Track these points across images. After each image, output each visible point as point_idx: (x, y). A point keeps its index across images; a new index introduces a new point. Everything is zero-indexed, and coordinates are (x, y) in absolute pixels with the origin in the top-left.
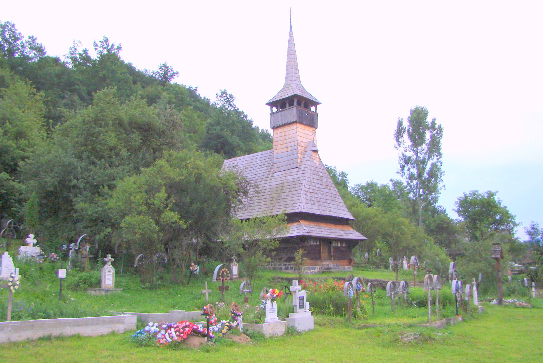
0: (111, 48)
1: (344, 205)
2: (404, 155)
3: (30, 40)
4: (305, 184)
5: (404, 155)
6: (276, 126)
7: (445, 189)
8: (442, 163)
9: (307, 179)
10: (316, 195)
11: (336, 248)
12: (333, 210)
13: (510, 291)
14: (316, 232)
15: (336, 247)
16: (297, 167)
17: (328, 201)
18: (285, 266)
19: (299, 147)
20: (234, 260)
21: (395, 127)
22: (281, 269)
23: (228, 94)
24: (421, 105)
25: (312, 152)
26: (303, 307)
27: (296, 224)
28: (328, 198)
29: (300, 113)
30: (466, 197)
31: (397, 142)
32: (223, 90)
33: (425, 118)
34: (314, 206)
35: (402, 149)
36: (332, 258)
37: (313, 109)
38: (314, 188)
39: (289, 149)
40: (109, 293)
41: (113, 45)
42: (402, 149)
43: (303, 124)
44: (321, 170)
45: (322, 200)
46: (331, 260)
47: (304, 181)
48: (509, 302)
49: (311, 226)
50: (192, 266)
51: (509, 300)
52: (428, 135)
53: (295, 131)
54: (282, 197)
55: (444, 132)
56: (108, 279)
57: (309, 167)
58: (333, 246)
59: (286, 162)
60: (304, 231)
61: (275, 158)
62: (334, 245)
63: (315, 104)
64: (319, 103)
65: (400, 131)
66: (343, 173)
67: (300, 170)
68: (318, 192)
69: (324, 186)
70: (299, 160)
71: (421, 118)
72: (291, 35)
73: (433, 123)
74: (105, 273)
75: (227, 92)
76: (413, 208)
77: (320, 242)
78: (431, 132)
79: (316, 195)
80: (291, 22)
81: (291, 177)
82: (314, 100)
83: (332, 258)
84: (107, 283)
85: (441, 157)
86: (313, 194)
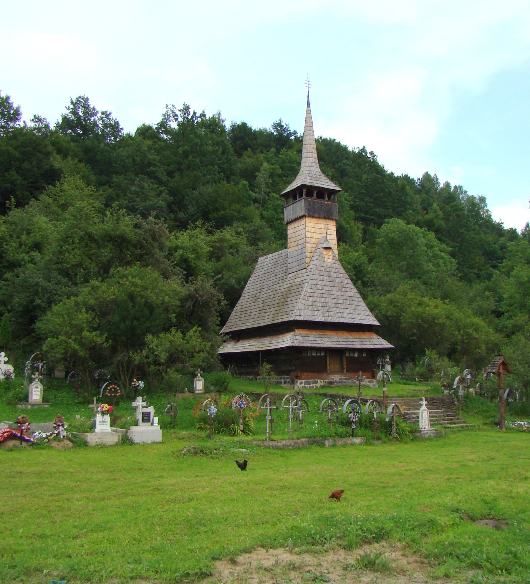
0: (192, 117)
3: (104, 116)
4: (307, 288)
9: (311, 282)
14: (314, 342)
17: (340, 306)
19: (307, 245)
20: (199, 374)
23: (368, 152)
25: (323, 250)
27: (292, 333)
29: (310, 205)
32: (361, 148)
34: (316, 313)
36: (345, 371)
38: (320, 291)
40: (36, 407)
41: (195, 113)
43: (316, 218)
44: (334, 270)
45: (330, 305)
46: (343, 372)
50: (134, 382)
53: (303, 227)
56: (35, 394)
60: (295, 341)
61: (289, 257)
62: (347, 355)
68: (326, 296)
69: (337, 289)
70: (308, 260)
72: (309, 112)
74: (32, 389)
75: (366, 149)
77: (326, 354)
80: (308, 97)
84: (34, 398)
86: (318, 299)
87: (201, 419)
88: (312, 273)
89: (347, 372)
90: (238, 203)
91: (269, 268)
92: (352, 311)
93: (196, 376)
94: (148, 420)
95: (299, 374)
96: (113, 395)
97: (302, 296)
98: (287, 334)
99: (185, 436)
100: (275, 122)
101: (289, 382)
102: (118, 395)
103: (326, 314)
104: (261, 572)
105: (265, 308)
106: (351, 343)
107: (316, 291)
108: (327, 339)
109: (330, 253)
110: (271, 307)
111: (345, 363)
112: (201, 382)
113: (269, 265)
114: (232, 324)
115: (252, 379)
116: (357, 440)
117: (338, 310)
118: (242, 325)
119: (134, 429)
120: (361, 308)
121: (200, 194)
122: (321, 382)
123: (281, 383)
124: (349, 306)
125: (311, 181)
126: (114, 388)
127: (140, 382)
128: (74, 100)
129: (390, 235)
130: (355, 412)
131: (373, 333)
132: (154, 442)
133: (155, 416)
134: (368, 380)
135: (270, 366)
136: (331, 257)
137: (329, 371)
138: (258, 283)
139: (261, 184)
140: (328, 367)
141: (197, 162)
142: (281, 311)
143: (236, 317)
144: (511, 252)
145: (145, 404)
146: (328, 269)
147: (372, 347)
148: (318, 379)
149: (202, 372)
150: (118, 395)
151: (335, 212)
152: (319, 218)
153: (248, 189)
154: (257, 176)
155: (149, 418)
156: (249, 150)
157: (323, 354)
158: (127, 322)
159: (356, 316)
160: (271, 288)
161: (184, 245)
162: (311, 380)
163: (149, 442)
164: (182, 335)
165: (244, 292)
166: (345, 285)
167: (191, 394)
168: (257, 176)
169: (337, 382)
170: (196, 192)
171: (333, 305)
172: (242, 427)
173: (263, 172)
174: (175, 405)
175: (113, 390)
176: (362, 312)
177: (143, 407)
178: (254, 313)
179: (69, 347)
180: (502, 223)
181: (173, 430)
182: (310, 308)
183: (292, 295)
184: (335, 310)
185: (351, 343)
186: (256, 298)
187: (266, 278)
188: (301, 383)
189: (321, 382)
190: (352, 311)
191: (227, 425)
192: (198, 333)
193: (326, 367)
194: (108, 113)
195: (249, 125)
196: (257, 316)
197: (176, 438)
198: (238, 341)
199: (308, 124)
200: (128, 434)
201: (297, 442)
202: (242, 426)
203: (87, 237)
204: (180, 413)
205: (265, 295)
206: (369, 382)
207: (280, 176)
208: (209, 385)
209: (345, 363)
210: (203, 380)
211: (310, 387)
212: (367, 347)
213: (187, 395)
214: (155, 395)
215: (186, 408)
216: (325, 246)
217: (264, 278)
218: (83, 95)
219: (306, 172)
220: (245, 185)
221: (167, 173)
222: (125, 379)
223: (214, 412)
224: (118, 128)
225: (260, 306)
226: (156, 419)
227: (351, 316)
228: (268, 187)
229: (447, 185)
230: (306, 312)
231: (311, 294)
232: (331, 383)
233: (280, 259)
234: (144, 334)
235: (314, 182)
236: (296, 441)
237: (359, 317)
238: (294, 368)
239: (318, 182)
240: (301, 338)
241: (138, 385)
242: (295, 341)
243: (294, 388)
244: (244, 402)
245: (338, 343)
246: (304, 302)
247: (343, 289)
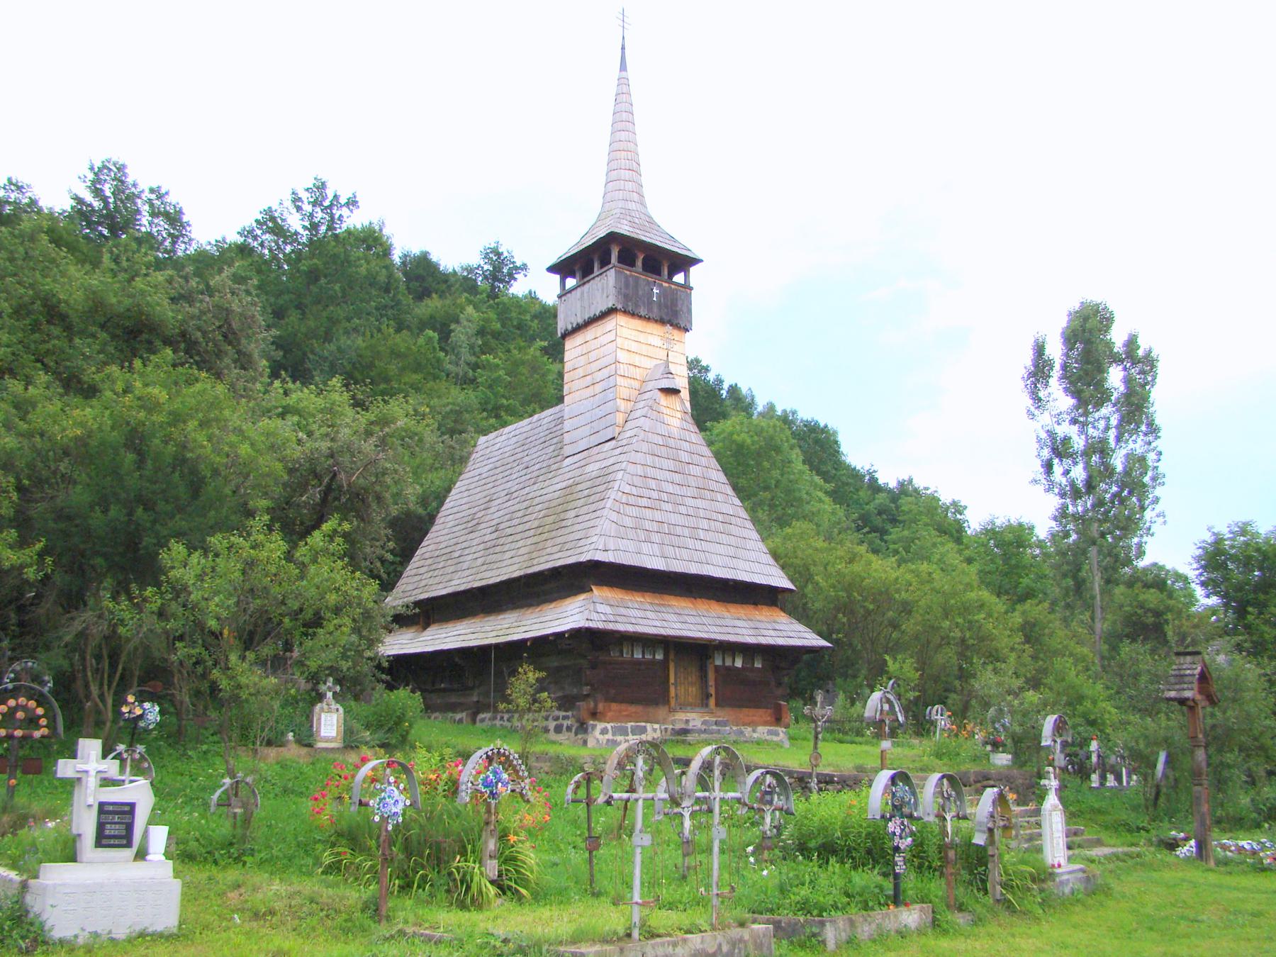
1: (761, 545)
2: (1051, 434)
4: (621, 482)
5: (1051, 434)
6: (570, 328)
7: (1165, 522)
8: (1160, 453)
9: (631, 468)
10: (658, 516)
11: (727, 674)
12: (716, 559)
13: (1259, 812)
14: (641, 621)
15: (728, 668)
16: (613, 438)
17: (702, 534)
18: (555, 723)
19: (620, 381)
21: (1027, 359)
22: (546, 730)
24: (1095, 296)
25: (659, 393)
26: (125, 842)
27: (582, 597)
28: (705, 524)
29: (627, 285)
30: (1218, 540)
31: (1033, 399)
33: (1107, 328)
34: (646, 548)
35: (1045, 419)
36: (712, 701)
37: (679, 278)
38: (655, 495)
39: (598, 388)
42: (1045, 419)
43: (640, 317)
44: (686, 446)
45: (679, 530)
47: (620, 475)
48: (1240, 849)
49: (630, 604)
51: (1241, 843)
52: (1115, 377)
53: (611, 336)
54: (564, 523)
55: (1161, 368)
57: (642, 434)
58: (717, 668)
59: (589, 426)
60: (595, 616)
62: (718, 662)
63: (683, 262)
64: (695, 261)
65: (1039, 370)
66: (954, 502)
67: (620, 443)
68: (669, 507)
69: (695, 492)
70: (620, 418)
71: (1090, 331)
72: (623, 82)
73: (1131, 343)
76: (1075, 577)
78: (1125, 369)
79: (658, 516)
80: (623, 48)
81: (597, 465)
82: (679, 251)
83: (712, 701)
85: (1157, 437)
86: (648, 513)
87: (340, 834)
88: (635, 447)
89: (717, 705)
90: (415, 372)
91: (507, 455)
92: (731, 551)
93: (320, 697)
94: (125, 839)
95: (601, 706)
96: (19, 733)
97: (610, 501)
98: (569, 601)
99: (278, 905)
100: (488, 246)
101: (569, 729)
102: (37, 734)
103: (670, 551)
105: (501, 541)
106: (730, 630)
107: (646, 493)
108: (672, 617)
109: (672, 401)
110: (518, 537)
111: (711, 682)
112: (335, 716)
113: (507, 449)
114: (410, 587)
115: (461, 721)
116: (911, 917)
117: (698, 545)
118: (441, 586)
119: (56, 875)
120: (750, 545)
121: (339, 349)
122: (655, 730)
123: (546, 730)
124: (724, 539)
125: (631, 229)
126: (24, 708)
127: (147, 705)
128: (98, 164)
129: (735, 437)
130: (902, 816)
131: (777, 610)
132: (142, 935)
133: (152, 821)
135: (539, 675)
136: (679, 415)
137: (673, 702)
138: (478, 489)
139: (460, 346)
141: (335, 291)
142: (549, 543)
143: (422, 570)
144: (908, 513)
145: (111, 767)
146: (671, 442)
147: (781, 642)
148: (647, 722)
149: (338, 688)
150: (37, 734)
152: (648, 319)
153: (437, 346)
154: (452, 331)
155: (130, 827)
156: (434, 295)
158: (114, 512)
159: (741, 564)
160: (515, 495)
161: (302, 405)
162: (629, 725)
163: (121, 933)
164: (284, 546)
165: (440, 515)
166: (713, 486)
167: (305, 750)
168: (452, 331)
169: (701, 732)
170: (332, 347)
171: (686, 532)
172: (492, 868)
173: (465, 323)
174: (249, 779)
175: (20, 715)
176: (753, 555)
177: (107, 782)
178: (470, 557)
179: (14, 637)
180: (875, 471)
181: (233, 874)
182: (631, 534)
183: (581, 502)
184: (690, 543)
185: (730, 630)
186: (474, 522)
187: (500, 476)
188: (604, 732)
189: (655, 730)
190: (731, 551)
191: (439, 858)
192: (338, 545)
193: (667, 690)
194: (163, 191)
195: (434, 258)
196: (480, 561)
197: (241, 910)
198: (425, 628)
199: (623, 107)
200: (29, 899)
201: (741, 940)
202: (495, 862)
203: (38, 306)
204: (264, 808)
205: (501, 513)
206: (770, 733)
207: (496, 335)
208: (357, 726)
209: (711, 682)
210: (341, 710)
212: (771, 641)
213: (292, 752)
214: (195, 749)
215: (286, 791)
216: (666, 384)
217: (494, 478)
218: (114, 159)
219: (618, 211)
220: (430, 339)
221: (273, 310)
222: (102, 696)
223: (399, 808)
224: (180, 220)
225: (487, 538)
226: (159, 837)
228: (474, 354)
229: (771, 407)
230: (622, 544)
231: (632, 500)
232: (685, 732)
233: (536, 431)
234: (163, 543)
235: (638, 231)
236: (736, 932)
237: (747, 566)
238: (586, 689)
239: (647, 234)
240: (608, 610)
241: (141, 717)
242: (595, 616)
243: (585, 743)
244: (505, 776)
245: (700, 627)
246: (614, 516)
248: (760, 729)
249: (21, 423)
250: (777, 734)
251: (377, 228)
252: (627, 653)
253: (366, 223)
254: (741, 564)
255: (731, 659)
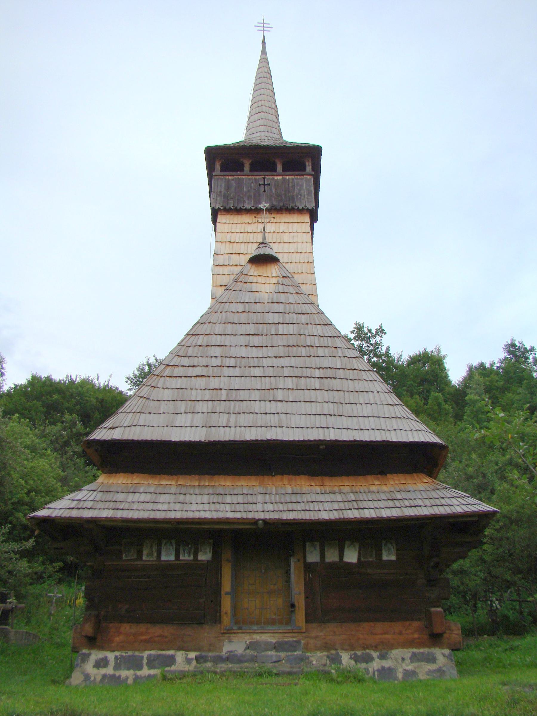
36: (300, 616)
45: (243, 395)
46: (290, 621)
62: (313, 557)
72: (264, 52)
80: (264, 42)
86: (201, 383)
89: (308, 620)
92: (329, 408)
104: (508, 652)
122: (189, 661)
134: (407, 653)
137: (226, 620)
140: (227, 604)
148: (179, 649)
151: (304, 192)
157: (205, 556)
159: (344, 422)
162: (146, 654)
188: (99, 664)
206: (414, 658)
211: (137, 678)
227: (322, 421)
247: (304, 351)
248: (396, 653)
249: (67, 403)
250: (432, 659)
251: (435, 353)
252: (150, 554)
253: (422, 350)
254: (244, 420)
255: (337, 553)
